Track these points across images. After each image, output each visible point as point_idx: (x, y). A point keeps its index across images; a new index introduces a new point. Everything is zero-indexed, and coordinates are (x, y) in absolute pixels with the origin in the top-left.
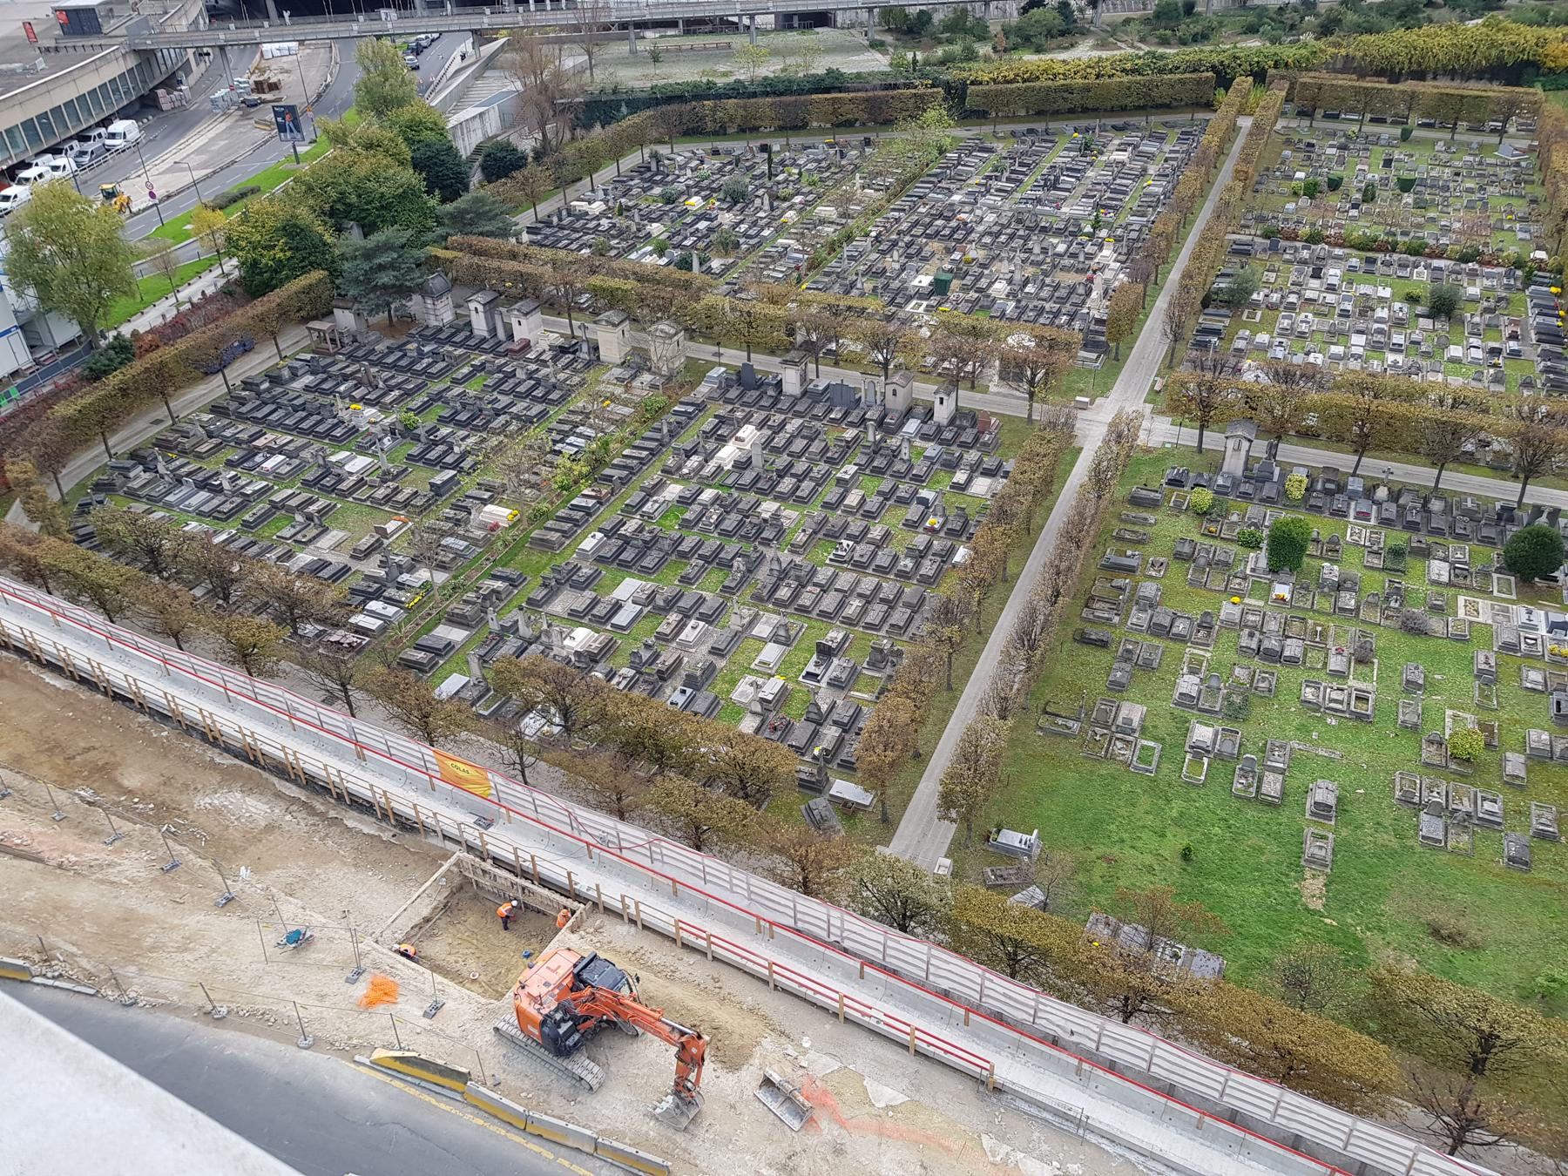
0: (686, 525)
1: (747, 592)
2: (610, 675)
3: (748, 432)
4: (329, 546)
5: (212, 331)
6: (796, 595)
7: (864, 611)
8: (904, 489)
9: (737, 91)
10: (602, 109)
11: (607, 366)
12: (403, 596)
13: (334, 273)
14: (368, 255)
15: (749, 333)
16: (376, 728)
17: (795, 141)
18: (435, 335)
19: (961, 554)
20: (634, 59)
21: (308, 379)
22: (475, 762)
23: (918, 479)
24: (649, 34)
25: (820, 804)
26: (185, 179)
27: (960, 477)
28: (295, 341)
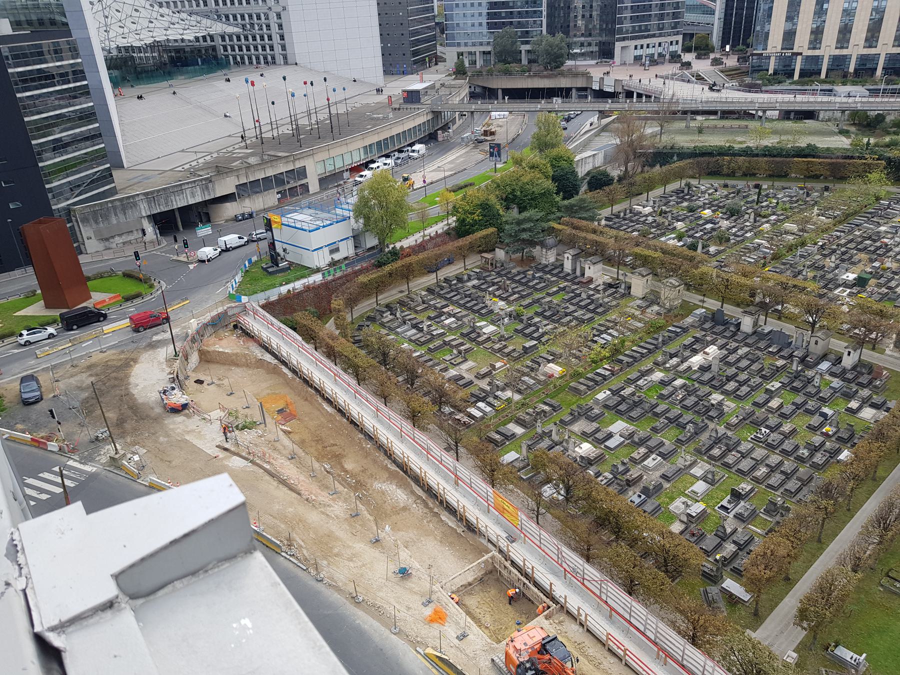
0: (662, 397)
1: (692, 447)
2: (598, 474)
3: (712, 350)
4: (466, 370)
5: (437, 251)
6: (723, 455)
7: (768, 476)
8: (811, 404)
9: (747, 152)
10: (662, 157)
11: (634, 298)
12: (496, 403)
13: (500, 230)
14: (519, 223)
15: (725, 292)
16: (467, 471)
17: (778, 184)
18: (543, 269)
19: (845, 455)
20: (687, 131)
21: (475, 282)
22: (515, 502)
23: (823, 400)
24: (699, 118)
25: (713, 590)
26: (441, 175)
27: (854, 404)
28: (474, 262)
